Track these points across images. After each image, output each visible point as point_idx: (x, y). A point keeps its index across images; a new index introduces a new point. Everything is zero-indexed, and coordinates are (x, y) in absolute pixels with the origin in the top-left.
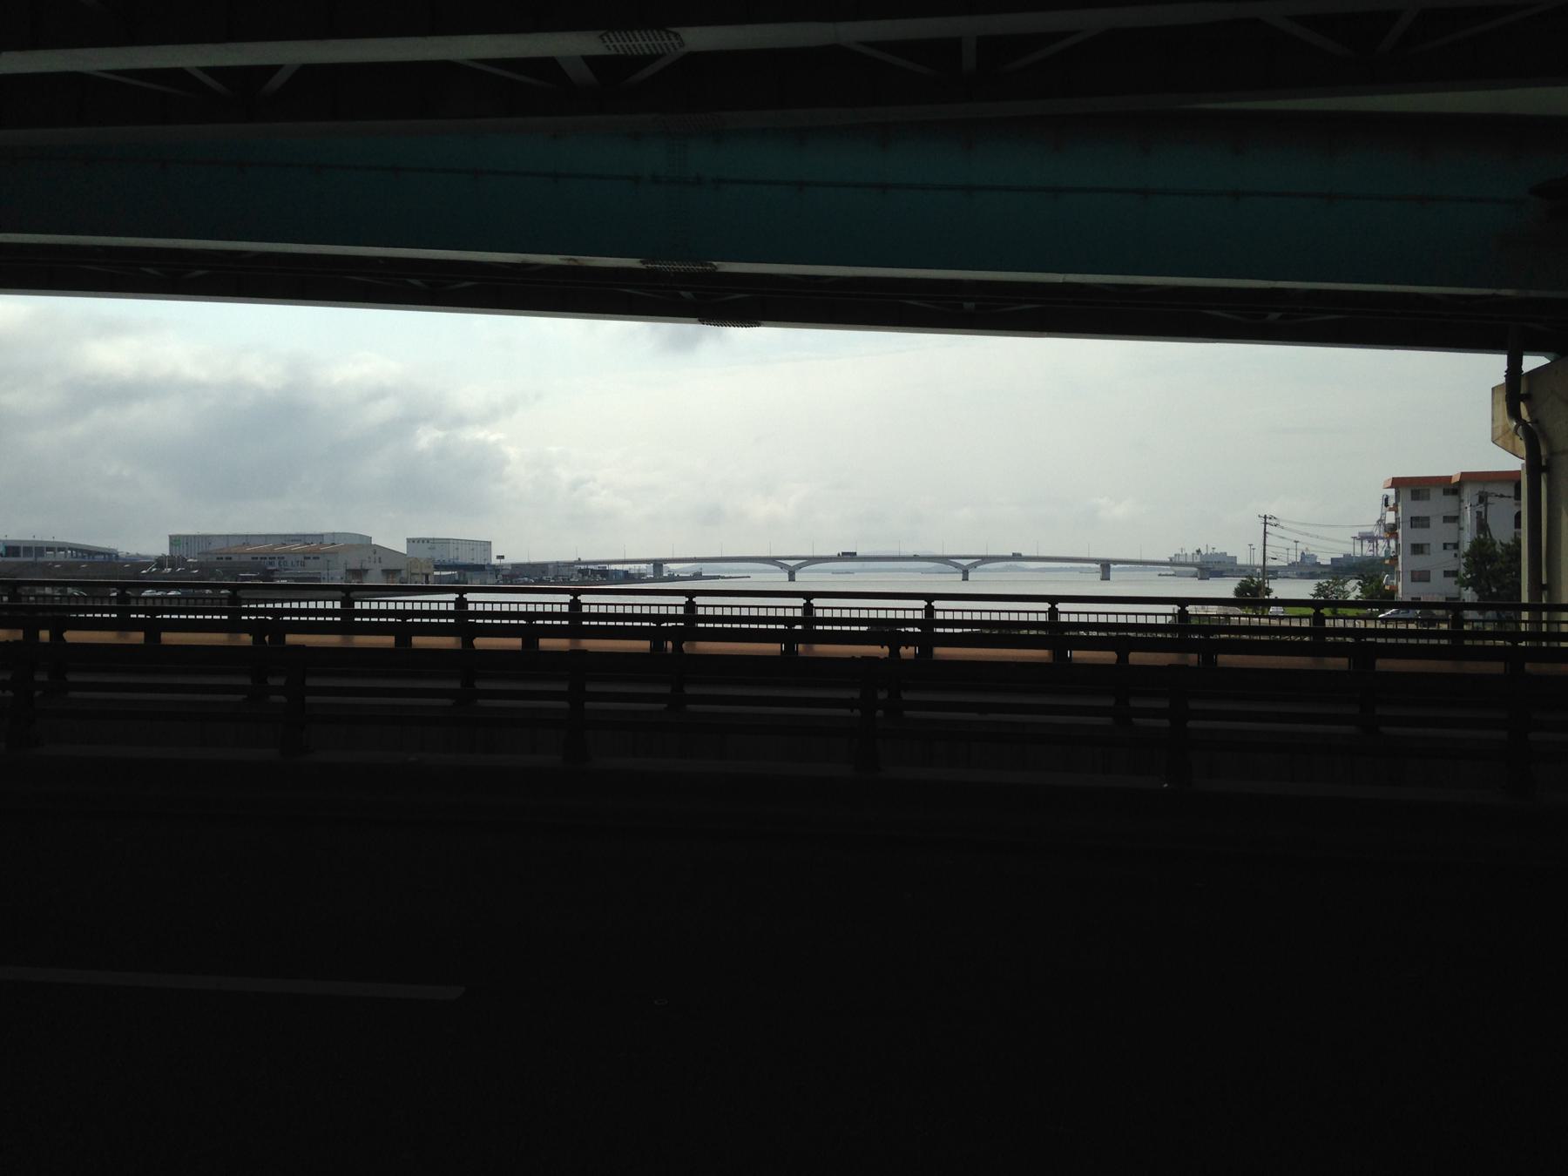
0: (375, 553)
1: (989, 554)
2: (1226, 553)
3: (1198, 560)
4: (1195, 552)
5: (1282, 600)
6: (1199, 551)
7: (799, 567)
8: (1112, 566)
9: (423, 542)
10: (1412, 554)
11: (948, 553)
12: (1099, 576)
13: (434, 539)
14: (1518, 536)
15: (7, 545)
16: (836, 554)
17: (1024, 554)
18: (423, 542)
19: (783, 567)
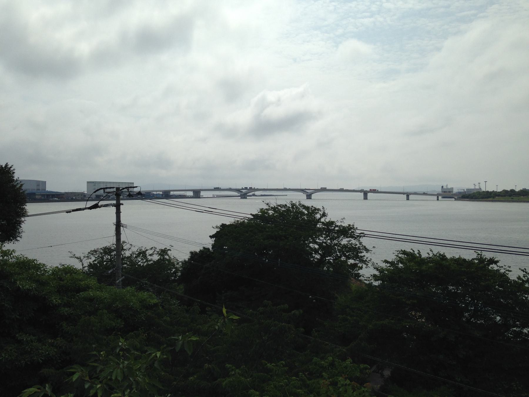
6: (442, 187)
13: (95, 182)
18: (92, 183)
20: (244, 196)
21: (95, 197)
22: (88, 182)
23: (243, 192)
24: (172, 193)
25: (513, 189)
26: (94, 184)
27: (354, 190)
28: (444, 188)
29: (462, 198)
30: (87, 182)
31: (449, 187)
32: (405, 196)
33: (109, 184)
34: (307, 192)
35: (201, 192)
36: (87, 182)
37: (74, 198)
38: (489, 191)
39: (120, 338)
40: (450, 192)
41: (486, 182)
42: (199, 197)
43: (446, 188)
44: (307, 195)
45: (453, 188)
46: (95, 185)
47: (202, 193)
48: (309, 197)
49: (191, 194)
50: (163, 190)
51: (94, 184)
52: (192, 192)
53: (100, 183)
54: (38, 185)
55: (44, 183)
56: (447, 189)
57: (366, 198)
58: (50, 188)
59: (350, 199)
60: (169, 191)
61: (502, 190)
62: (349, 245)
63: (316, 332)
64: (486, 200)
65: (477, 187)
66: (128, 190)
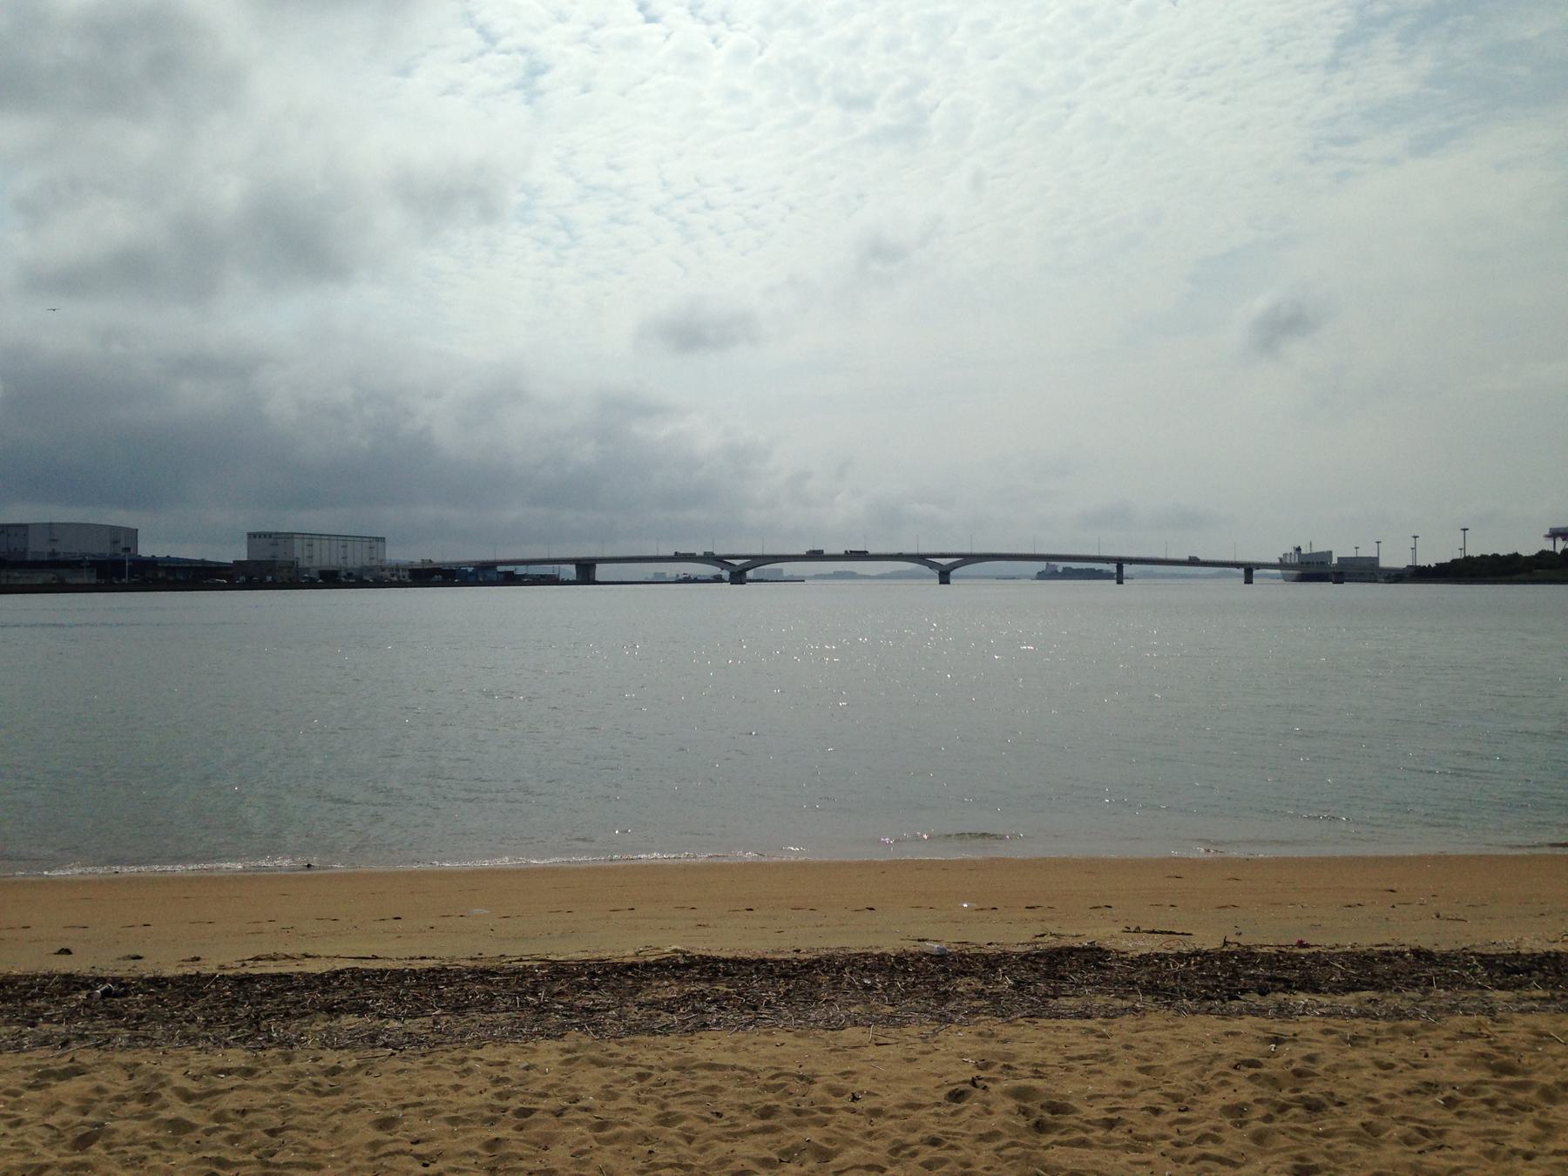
0: (1156, 1111)
1: (1237, 560)
2: (822, 551)
3: (1295, 560)
4: (1292, 551)
5: (683, 554)
6: (1299, 549)
7: (954, 566)
8: (1255, 572)
9: (265, 536)
10: (1551, 529)
11: (923, 550)
12: (1243, 580)
13: (277, 533)
14: (470, 971)
15: (322, 569)
16: (843, 553)
17: (1202, 558)
18: (260, 537)
19: (932, 566)
22: (249, 535)
23: (735, 565)
25: (1542, 551)
27: (901, 554)
28: (1303, 552)
29: (1038, 579)
30: (249, 534)
31: (1316, 549)
32: (1241, 571)
33: (327, 541)
34: (730, 564)
35: (598, 566)
36: (249, 534)
38: (1501, 554)
39: (1232, 1117)
41: (1465, 530)
43: (1308, 552)
46: (277, 545)
47: (601, 571)
49: (570, 571)
52: (574, 566)
53: (303, 538)
54: (115, 542)
55: (133, 534)
57: (1249, 580)
59: (1181, 581)
61: (1479, 555)
63: (33, 1025)
66: (1120, 568)
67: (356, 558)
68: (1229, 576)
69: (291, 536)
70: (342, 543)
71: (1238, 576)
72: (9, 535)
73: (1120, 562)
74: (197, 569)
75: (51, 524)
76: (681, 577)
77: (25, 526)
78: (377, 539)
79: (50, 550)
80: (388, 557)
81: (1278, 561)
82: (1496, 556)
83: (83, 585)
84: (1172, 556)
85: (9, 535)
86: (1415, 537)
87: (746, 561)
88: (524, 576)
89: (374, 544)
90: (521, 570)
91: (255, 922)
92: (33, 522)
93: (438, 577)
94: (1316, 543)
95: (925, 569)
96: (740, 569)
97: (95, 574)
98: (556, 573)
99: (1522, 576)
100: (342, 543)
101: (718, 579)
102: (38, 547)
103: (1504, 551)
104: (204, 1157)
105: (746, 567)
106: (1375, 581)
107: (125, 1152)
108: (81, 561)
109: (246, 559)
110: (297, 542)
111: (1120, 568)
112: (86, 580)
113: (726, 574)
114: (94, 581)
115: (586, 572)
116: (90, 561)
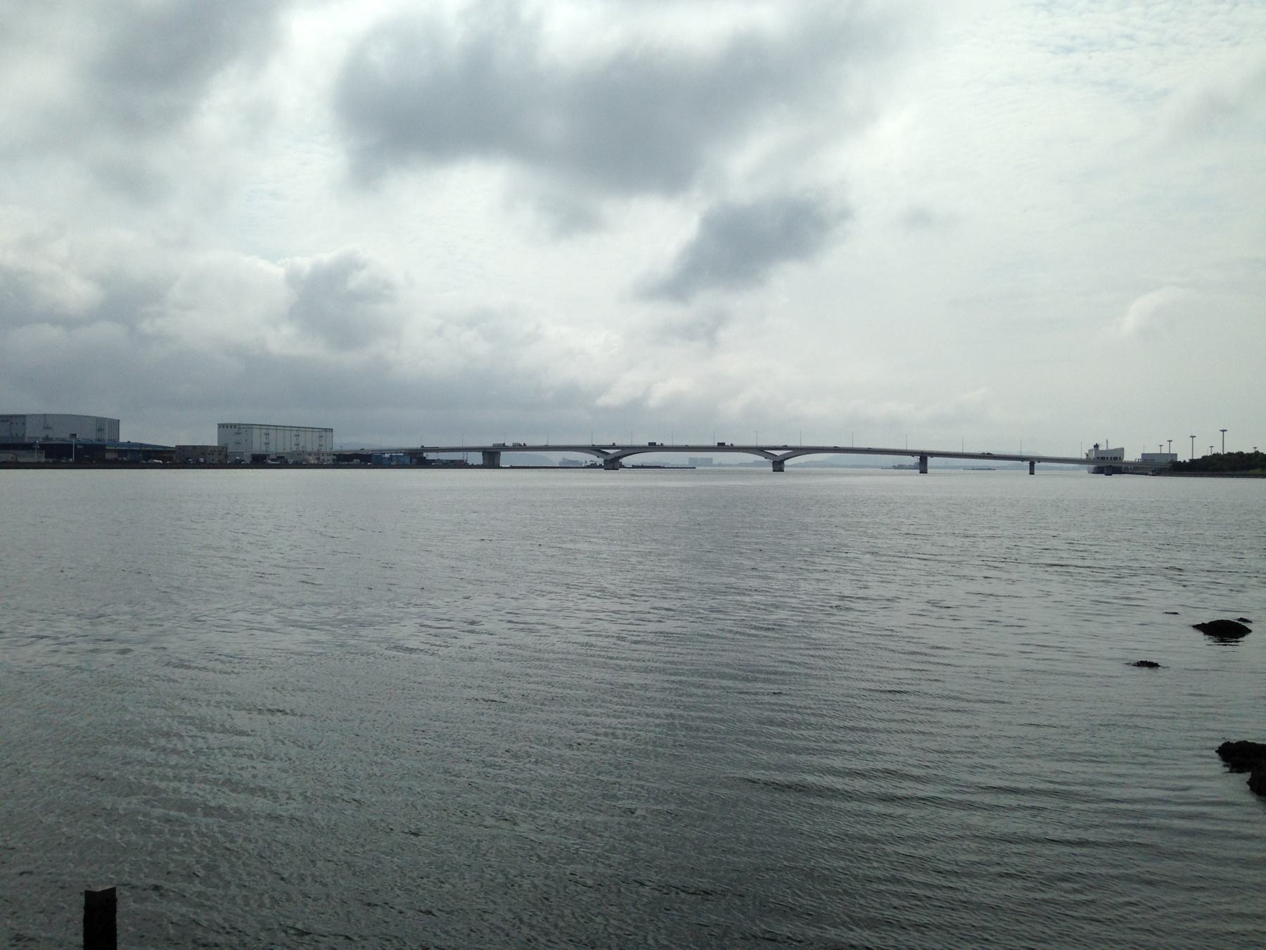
8: (1037, 464)
13: (240, 424)
19: (768, 456)
20: (612, 465)
21: (251, 460)
24: (431, 456)
26: (236, 430)
28: (1100, 448)
30: (219, 425)
31: (1112, 446)
32: (1027, 464)
36: (219, 425)
37: (202, 460)
38: (1245, 452)
40: (1116, 458)
41: (1223, 431)
42: (496, 466)
44: (774, 462)
45: (1123, 449)
46: (239, 433)
47: (505, 458)
48: (778, 466)
49: (477, 458)
50: (406, 450)
51: (236, 430)
54: (100, 430)
55: (115, 424)
56: (1107, 451)
58: (129, 434)
60: (424, 449)
62: (86, 787)
64: (1244, 472)
65: (1165, 451)
66: (1032, 465)
67: (310, 444)
68: (1016, 468)
69: (250, 426)
70: (264, 431)
71: (1023, 468)
72: (12, 423)
73: (924, 457)
74: (149, 451)
75: (45, 415)
76: (589, 464)
77: (24, 416)
78: (326, 430)
79: (44, 436)
80: (28, 435)
81: (1084, 457)
82: (1240, 454)
83: (29, 463)
84: (857, 445)
85: (12, 423)
86: (1193, 437)
87: (617, 451)
88: (434, 461)
89: (323, 434)
90: (880, 470)
91: (1003, 703)
92: (31, 413)
93: (356, 461)
94: (1110, 442)
95: (761, 458)
96: (780, 459)
97: (44, 455)
98: (465, 459)
99: (1258, 471)
100: (264, 431)
101: (593, 466)
102: (33, 433)
103: (1248, 449)
104: (1126, 869)
105: (786, 457)
106: (1146, 474)
107: (869, 911)
108: (32, 444)
109: (216, 444)
110: (256, 432)
111: (1032, 465)
112: (35, 460)
113: (600, 461)
114: (43, 460)
115: (491, 458)
116: (40, 445)
